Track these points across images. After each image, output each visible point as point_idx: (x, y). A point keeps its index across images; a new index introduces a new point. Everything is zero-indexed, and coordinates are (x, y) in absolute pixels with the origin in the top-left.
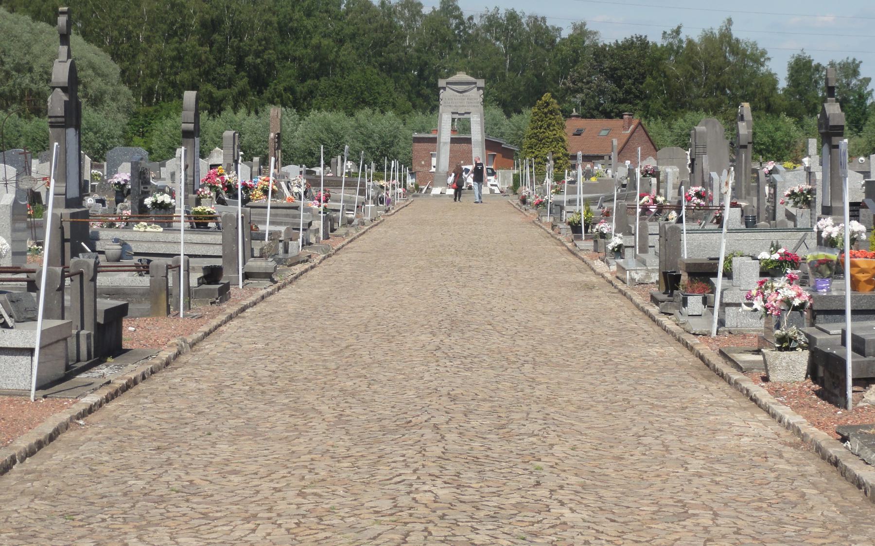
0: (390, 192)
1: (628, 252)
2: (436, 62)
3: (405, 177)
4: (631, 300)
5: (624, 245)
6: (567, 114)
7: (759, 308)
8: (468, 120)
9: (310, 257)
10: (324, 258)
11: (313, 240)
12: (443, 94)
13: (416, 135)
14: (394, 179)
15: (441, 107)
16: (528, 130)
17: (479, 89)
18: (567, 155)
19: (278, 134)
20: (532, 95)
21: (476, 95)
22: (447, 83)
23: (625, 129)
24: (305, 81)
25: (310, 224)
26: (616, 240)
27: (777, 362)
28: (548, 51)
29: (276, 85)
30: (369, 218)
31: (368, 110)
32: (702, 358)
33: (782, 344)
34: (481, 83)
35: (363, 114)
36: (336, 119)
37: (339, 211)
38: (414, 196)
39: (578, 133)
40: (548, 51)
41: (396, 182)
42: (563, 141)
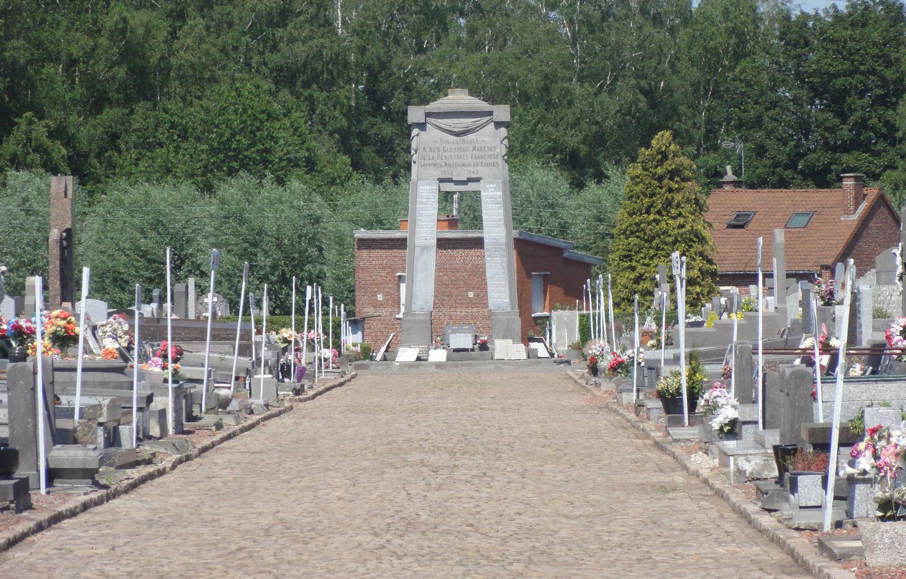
0: (305, 356)
1: (747, 432)
2: (405, 62)
3: (337, 326)
4: (728, 500)
5: (741, 419)
6: (714, 178)
7: (868, 468)
8: (476, 196)
9: (154, 455)
10: (180, 461)
11: (155, 431)
12: (418, 139)
13: (362, 233)
14: (311, 328)
15: (414, 167)
16: (620, 217)
17: (498, 125)
18: (714, 274)
19: (68, 231)
20: (627, 138)
21: (492, 140)
22: (428, 115)
23: (847, 212)
24: (100, 112)
25: (150, 399)
26: (728, 412)
27: (877, 537)
28: (672, 30)
29: (30, 123)
30: (261, 401)
31: (245, 179)
32: (791, 553)
33: (885, 512)
34: (502, 112)
35: (231, 190)
36: (169, 197)
37: (200, 381)
38: (357, 367)
39: (739, 223)
40: (672, 30)
41: (317, 334)
42: (702, 240)
